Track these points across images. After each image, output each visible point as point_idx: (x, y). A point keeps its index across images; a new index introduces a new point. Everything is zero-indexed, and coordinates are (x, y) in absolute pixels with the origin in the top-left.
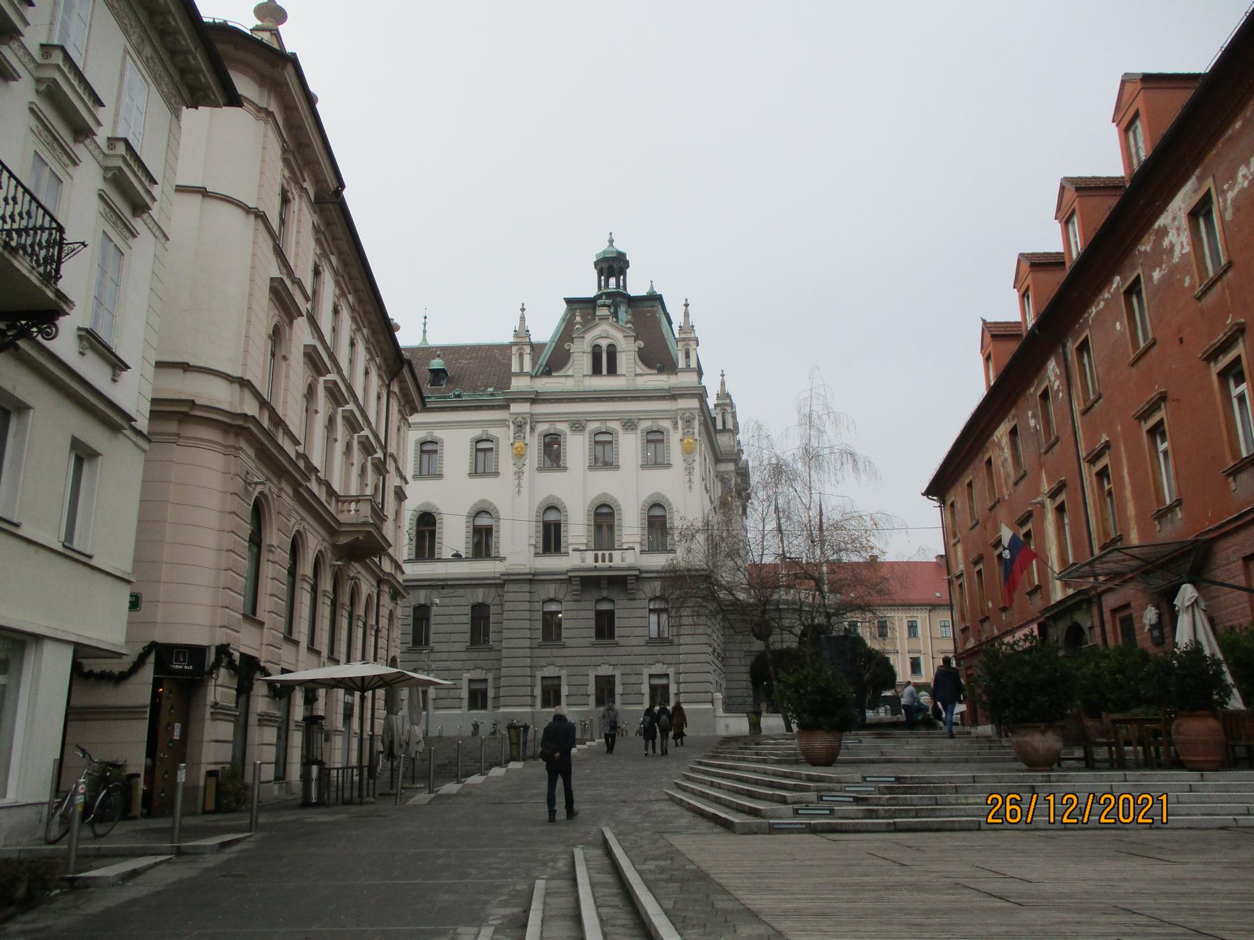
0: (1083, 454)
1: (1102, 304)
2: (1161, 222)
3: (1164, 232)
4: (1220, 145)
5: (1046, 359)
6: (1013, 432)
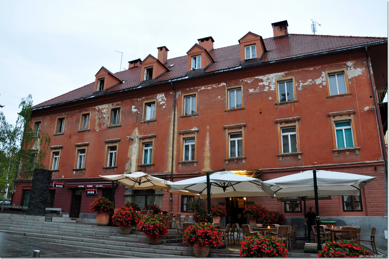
0: (176, 130)
1: (209, 88)
2: (260, 77)
3: (262, 81)
4: (300, 70)
5: (160, 92)
6: (115, 111)
